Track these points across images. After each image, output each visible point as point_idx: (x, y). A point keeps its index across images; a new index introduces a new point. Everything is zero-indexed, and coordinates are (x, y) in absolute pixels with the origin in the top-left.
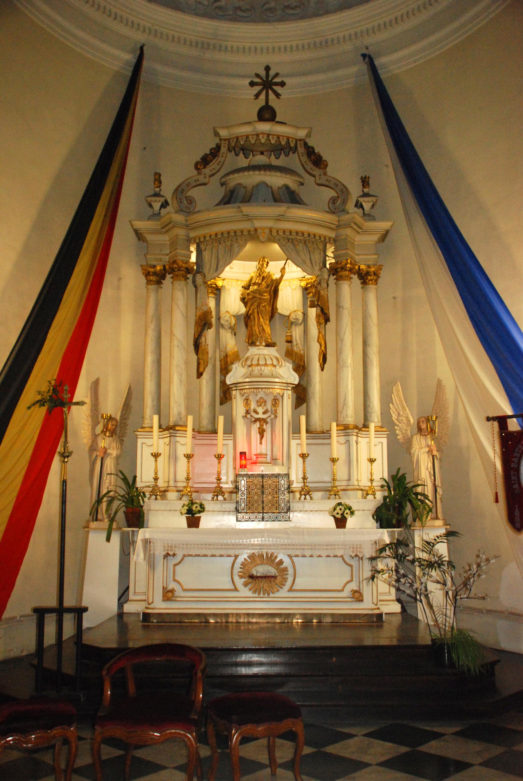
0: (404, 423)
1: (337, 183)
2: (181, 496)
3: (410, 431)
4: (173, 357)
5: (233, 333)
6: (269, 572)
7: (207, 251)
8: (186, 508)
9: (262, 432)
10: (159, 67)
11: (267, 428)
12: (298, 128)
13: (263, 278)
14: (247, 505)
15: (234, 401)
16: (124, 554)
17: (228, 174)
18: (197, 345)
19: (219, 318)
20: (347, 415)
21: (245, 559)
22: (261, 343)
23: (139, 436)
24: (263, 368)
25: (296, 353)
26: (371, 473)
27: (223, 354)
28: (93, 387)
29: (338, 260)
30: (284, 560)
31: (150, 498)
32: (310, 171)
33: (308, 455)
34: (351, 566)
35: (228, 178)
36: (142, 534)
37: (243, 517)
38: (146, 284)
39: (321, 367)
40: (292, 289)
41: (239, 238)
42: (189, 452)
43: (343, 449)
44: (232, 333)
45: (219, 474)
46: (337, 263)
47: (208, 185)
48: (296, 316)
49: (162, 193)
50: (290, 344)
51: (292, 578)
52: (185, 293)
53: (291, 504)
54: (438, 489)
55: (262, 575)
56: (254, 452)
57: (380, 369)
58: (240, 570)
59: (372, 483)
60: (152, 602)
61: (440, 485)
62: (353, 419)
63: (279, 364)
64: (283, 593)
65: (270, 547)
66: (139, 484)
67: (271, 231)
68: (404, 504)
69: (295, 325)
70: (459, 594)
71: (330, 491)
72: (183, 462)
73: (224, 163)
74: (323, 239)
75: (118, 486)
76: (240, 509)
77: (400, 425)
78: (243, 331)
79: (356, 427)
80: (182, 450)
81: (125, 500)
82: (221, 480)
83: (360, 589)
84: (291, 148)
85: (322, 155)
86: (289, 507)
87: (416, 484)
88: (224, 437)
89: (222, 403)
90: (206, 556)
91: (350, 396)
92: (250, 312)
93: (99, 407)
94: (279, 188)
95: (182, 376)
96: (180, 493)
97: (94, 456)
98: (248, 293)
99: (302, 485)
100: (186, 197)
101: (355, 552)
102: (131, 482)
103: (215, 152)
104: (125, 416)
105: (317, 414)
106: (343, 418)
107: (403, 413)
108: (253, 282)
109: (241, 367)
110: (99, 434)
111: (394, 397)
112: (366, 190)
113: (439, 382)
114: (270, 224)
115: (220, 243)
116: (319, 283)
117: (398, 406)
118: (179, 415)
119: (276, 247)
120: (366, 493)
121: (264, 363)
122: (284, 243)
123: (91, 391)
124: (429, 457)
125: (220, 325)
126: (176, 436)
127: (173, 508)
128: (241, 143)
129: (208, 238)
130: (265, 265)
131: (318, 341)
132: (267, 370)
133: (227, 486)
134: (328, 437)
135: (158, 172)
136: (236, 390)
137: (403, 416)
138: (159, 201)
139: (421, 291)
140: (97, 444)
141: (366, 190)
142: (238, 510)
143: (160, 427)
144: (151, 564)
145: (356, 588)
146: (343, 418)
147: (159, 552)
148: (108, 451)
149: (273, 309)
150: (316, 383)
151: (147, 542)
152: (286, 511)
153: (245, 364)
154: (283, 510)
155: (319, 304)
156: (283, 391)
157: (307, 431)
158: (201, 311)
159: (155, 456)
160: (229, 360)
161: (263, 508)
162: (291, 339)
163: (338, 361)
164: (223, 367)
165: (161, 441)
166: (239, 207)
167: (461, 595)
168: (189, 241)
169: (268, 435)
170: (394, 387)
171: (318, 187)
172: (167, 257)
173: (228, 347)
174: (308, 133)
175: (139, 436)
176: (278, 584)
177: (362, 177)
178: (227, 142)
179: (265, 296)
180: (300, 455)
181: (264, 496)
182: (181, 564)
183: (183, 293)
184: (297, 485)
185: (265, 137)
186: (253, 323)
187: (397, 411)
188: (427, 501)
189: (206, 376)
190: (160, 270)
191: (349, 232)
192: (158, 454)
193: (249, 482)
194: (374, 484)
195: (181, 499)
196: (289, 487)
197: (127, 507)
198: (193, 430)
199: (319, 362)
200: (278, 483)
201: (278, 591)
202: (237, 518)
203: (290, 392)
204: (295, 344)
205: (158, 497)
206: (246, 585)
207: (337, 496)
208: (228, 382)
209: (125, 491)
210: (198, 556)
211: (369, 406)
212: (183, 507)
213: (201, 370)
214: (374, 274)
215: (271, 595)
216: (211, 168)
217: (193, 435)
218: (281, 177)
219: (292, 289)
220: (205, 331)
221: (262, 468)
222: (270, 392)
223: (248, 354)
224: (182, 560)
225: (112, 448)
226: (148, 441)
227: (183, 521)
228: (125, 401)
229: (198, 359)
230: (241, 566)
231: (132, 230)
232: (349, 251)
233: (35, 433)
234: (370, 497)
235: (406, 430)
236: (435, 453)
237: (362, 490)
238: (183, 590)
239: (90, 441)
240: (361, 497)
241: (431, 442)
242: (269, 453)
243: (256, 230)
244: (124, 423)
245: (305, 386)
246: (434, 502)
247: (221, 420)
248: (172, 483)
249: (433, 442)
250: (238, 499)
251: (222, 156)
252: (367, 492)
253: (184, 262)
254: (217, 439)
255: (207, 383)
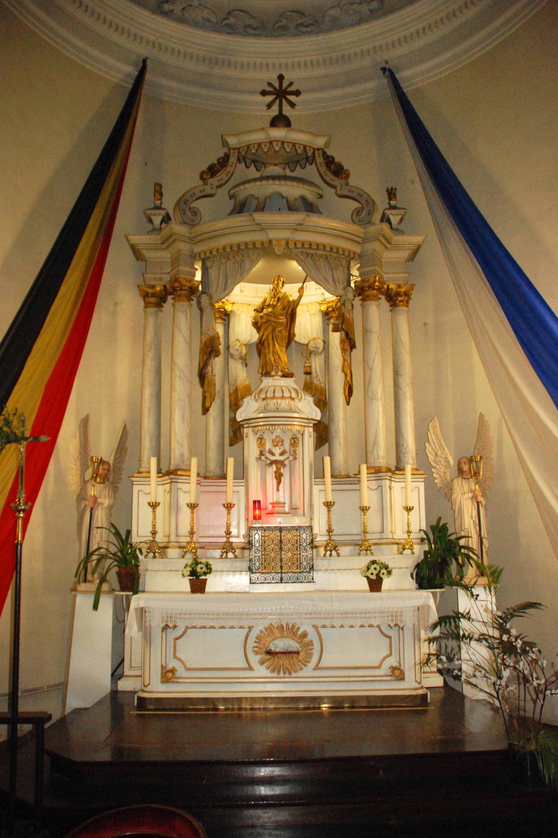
0: (442, 465)
1: (361, 192)
2: (183, 554)
3: (450, 475)
4: (174, 390)
5: (244, 364)
6: (290, 646)
7: (213, 269)
8: (189, 569)
9: (279, 477)
10: (164, 82)
11: (285, 471)
12: (316, 135)
13: (279, 299)
14: (262, 564)
15: (246, 440)
16: (118, 621)
17: (238, 185)
18: (202, 377)
19: (228, 347)
20: (378, 456)
21: (261, 631)
22: (277, 373)
23: (134, 483)
24: (279, 401)
25: (316, 386)
26: (408, 523)
27: (233, 388)
28: (82, 425)
29: (364, 277)
30: (308, 631)
31: (147, 555)
32: (331, 182)
33: (334, 503)
34: (389, 637)
35: (237, 189)
36: (137, 601)
37: (258, 578)
38: (145, 307)
39: (346, 400)
40: (310, 314)
41: (251, 252)
42: (193, 502)
43: (375, 495)
44: (243, 363)
45: (228, 526)
46: (363, 281)
47: (215, 196)
48: (316, 344)
49: (163, 206)
50: (309, 376)
51: (319, 654)
52: (189, 315)
53: (314, 562)
54: (484, 540)
55: (282, 650)
56: (270, 500)
57: (414, 402)
58: (255, 645)
59: (409, 536)
60: (149, 684)
61: (486, 537)
62: (385, 461)
63: (298, 396)
64: (308, 671)
65: (292, 617)
66: (135, 539)
67: (287, 243)
68: (448, 560)
69: (315, 355)
70: (548, 687)
71: (360, 546)
72: (186, 512)
73: (233, 173)
74: (347, 254)
75: (111, 543)
76: (254, 569)
77: (438, 466)
78: (255, 361)
79: (389, 470)
80: (184, 499)
81: (117, 558)
82: (232, 534)
83: (400, 665)
84: (307, 158)
85: (343, 164)
86: (313, 566)
87: (459, 535)
88: (234, 483)
89: (231, 444)
90: (212, 627)
91: (381, 433)
92: (264, 338)
93: (89, 449)
94: (296, 199)
95: (184, 412)
96: (182, 550)
97: (83, 506)
98: (261, 317)
99: (327, 538)
100: (190, 209)
101: (394, 620)
102: (124, 537)
103: (223, 162)
104: (120, 459)
105: (342, 455)
106: (374, 459)
107: (442, 453)
108: (267, 303)
109: (254, 402)
110: (88, 481)
111: (431, 434)
112: (393, 203)
113: (481, 416)
114: (286, 234)
115: (228, 258)
116: (344, 304)
117: (435, 445)
118: (181, 457)
119: (294, 266)
120: (402, 547)
121: (281, 395)
122: (302, 258)
123: (80, 430)
124: (473, 503)
125: (229, 355)
126: (178, 482)
127: (174, 569)
128: (253, 151)
129: (214, 253)
130: (281, 285)
131: (343, 371)
132: (284, 404)
133: (238, 540)
134: (357, 482)
135: (158, 182)
136: (248, 427)
137: (441, 457)
138: (160, 214)
139: (458, 316)
140: (86, 492)
141: (393, 203)
142: (252, 570)
143: (159, 471)
144: (147, 638)
145: (395, 664)
146: (374, 459)
147: (156, 623)
148: (99, 500)
149: (289, 334)
150: (339, 421)
151: (142, 611)
152: (308, 570)
153: (259, 397)
154: (305, 569)
155: (344, 327)
156: (303, 428)
157: (332, 476)
158: (207, 336)
159: (153, 506)
160: (239, 394)
161: (281, 567)
162: (311, 369)
163: (366, 393)
164: (233, 403)
165: (161, 488)
166: (251, 215)
167: (551, 690)
168: (194, 257)
169: (285, 479)
170: (431, 424)
171: (337, 198)
172: (168, 276)
173: (238, 379)
174: (326, 142)
175: (134, 483)
176: (302, 661)
177: (388, 189)
178: (236, 151)
179: (281, 319)
180: (324, 503)
181: (283, 553)
182: (183, 638)
183: (186, 316)
184: (321, 538)
185: (280, 144)
186: (267, 350)
187: (433, 450)
188: (471, 554)
189: (214, 411)
190: (160, 291)
191: (376, 246)
192: (156, 503)
193: (264, 536)
194: (412, 536)
195: (183, 557)
196: (312, 542)
197: (119, 567)
198: (198, 475)
199: (345, 395)
200: (299, 537)
201: (302, 669)
202: (250, 579)
203: (311, 430)
204: (315, 376)
205: (157, 554)
206: (262, 663)
207: (368, 552)
208: (239, 419)
209: (117, 547)
210: (204, 627)
211: (403, 445)
212: (185, 567)
213: (207, 404)
214: (405, 294)
215: (293, 674)
216: (219, 178)
217: (198, 480)
218: (299, 187)
219: (310, 314)
220: (212, 360)
221: (279, 520)
222: (288, 429)
223: (262, 386)
224: (184, 632)
225: (103, 497)
226: (146, 489)
227: (185, 584)
228: (120, 442)
229: (204, 392)
230: (257, 640)
231: (128, 247)
232: (377, 268)
233: (8, 480)
234: (407, 552)
235: (445, 473)
236: (480, 499)
237: (397, 544)
238: (186, 670)
239: (79, 488)
240: (396, 553)
241: (475, 487)
242: (287, 501)
243: (270, 241)
244: (120, 467)
245: (326, 423)
246: (480, 556)
247: (231, 462)
248: (173, 538)
249: (477, 486)
250: (251, 557)
251: (231, 166)
252: (404, 546)
253: (188, 280)
254: (226, 486)
255: (215, 420)
